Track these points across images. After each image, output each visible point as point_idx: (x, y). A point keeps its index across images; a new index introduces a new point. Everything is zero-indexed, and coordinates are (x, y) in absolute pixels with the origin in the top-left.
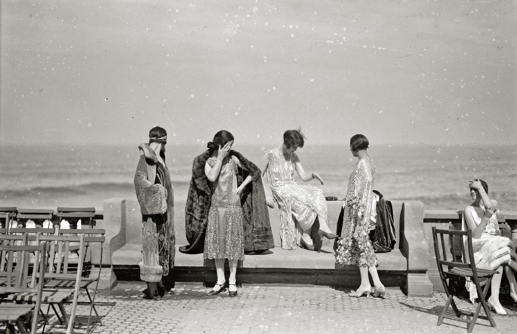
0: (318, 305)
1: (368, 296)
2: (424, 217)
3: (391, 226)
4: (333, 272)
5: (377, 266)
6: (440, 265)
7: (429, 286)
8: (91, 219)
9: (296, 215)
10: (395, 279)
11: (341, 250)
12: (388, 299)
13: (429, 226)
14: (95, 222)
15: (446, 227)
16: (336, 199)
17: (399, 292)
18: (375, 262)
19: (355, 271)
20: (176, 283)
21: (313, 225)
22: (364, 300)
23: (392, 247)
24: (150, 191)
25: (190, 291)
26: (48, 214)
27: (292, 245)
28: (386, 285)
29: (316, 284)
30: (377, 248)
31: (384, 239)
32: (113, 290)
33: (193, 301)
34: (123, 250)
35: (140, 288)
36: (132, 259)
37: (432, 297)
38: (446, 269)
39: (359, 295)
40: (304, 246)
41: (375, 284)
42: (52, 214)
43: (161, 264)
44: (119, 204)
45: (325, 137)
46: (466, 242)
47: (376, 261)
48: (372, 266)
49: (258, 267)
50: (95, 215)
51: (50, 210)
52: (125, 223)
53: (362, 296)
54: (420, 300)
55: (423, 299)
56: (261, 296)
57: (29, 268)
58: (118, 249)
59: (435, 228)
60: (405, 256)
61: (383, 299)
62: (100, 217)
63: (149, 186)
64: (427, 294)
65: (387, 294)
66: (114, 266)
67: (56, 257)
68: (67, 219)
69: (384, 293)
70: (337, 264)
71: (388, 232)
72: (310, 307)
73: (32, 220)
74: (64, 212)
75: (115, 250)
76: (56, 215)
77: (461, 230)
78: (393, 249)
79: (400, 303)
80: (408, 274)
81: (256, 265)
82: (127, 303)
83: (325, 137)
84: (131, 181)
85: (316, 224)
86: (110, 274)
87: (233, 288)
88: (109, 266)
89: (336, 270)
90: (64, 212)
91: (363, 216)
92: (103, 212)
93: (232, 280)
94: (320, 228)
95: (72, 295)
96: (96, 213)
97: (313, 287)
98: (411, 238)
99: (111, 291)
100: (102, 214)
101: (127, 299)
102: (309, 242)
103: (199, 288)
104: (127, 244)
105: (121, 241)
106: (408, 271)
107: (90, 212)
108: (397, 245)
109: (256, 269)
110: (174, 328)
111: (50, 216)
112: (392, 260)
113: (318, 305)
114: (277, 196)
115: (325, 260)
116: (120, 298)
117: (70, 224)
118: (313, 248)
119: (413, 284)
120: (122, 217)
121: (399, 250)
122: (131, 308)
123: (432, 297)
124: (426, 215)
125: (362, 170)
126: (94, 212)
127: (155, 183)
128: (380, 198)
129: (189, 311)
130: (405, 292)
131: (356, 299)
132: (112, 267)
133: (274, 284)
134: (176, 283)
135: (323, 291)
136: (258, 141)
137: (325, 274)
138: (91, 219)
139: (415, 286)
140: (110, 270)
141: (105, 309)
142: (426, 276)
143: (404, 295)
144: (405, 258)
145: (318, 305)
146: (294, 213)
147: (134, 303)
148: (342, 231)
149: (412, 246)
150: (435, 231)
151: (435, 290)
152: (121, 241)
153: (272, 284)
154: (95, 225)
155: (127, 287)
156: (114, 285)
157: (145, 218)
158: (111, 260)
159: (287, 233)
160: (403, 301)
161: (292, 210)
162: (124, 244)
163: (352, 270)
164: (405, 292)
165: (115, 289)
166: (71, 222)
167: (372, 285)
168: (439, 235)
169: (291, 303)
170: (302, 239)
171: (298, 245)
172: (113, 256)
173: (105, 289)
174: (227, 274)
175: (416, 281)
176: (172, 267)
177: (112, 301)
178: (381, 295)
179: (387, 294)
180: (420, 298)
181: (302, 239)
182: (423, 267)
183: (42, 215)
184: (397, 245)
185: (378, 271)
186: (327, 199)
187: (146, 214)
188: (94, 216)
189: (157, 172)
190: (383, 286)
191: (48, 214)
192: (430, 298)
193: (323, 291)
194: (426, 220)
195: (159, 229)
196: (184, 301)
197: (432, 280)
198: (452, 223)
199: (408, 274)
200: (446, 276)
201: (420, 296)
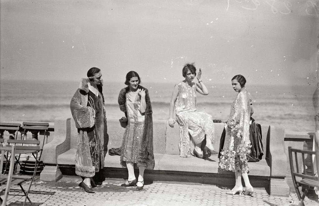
0: (202, 200)
1: (240, 194)
2: (285, 137)
3: (260, 143)
4: (215, 175)
5: (248, 172)
6: (294, 176)
7: (286, 188)
8: (46, 131)
9: (192, 132)
10: (262, 182)
11: (222, 159)
12: (256, 197)
13: (288, 144)
14: (49, 133)
15: (300, 146)
16: (220, 122)
17: (264, 191)
18: (247, 170)
19: (231, 175)
20: (106, 178)
21: (203, 141)
22: (237, 198)
23: (260, 157)
24: (83, 112)
25: (112, 184)
26: (17, 126)
27: (186, 154)
28: (254, 186)
29: (203, 183)
30: (249, 159)
31: (254, 152)
32: (58, 182)
33: (111, 193)
34: (67, 154)
35: (77, 181)
36: (71, 161)
37: (288, 197)
38: (299, 179)
39: (234, 193)
40: (196, 155)
41: (246, 185)
42: (20, 127)
43: (94, 164)
44: (65, 121)
45: (215, 76)
46: (314, 161)
47: (247, 169)
48: (244, 173)
49: (160, 170)
50: (49, 128)
51: (19, 124)
52: (70, 134)
53: (235, 194)
54: (280, 199)
55: (282, 198)
56: (162, 191)
57: (4, 163)
58: (63, 153)
59: (291, 147)
60: (268, 165)
61: (252, 196)
62: (52, 130)
63: (80, 108)
64: (285, 194)
65: (255, 193)
66: (59, 165)
67: (20, 156)
68: (30, 130)
69: (252, 193)
70: (219, 169)
71: (257, 148)
72: (196, 202)
73: (7, 130)
74: (27, 125)
75: (61, 154)
76: (22, 128)
77: (312, 150)
78: (261, 159)
79: (264, 201)
80: (271, 179)
81: (159, 168)
82: (64, 193)
83: (215, 76)
84: (69, 103)
85: (204, 142)
86: (56, 171)
87: (140, 184)
88: (55, 165)
89: (218, 174)
90: (27, 125)
91: (241, 136)
92: (54, 126)
93: (141, 178)
94: (206, 145)
95: (4, 191)
96: (49, 127)
97: (201, 185)
98: (276, 152)
99: (56, 183)
100: (53, 128)
101: (64, 190)
102: (200, 152)
103: (119, 183)
104: (71, 149)
105: (66, 147)
106: (271, 177)
107: (45, 126)
108: (264, 157)
109: (159, 171)
110: (155, 187)
111: (18, 128)
112: (259, 168)
113: (201, 200)
114: (179, 118)
115: (211, 166)
116: (60, 189)
117: (33, 134)
118: (202, 157)
119: (275, 187)
120: (67, 130)
121: (265, 160)
122: (64, 198)
123: (288, 197)
124: (287, 135)
125: (240, 100)
126: (48, 126)
127: (87, 106)
128: (252, 122)
129: (105, 201)
130: (269, 192)
131: (231, 196)
132: (57, 165)
133: (173, 182)
134: (106, 178)
135: (208, 188)
136: (162, 76)
137: (209, 176)
138: (46, 131)
139: (276, 188)
140: (56, 168)
141: (45, 198)
142: (285, 181)
143: (267, 194)
144: (269, 167)
145: (202, 200)
146: (190, 131)
147: (68, 193)
148: (224, 145)
149: (274, 159)
150: (291, 150)
151: (292, 191)
152: (66, 147)
153: (171, 182)
154: (49, 135)
155: (67, 179)
156: (60, 178)
157: (79, 130)
158: (56, 160)
159: (184, 145)
160: (267, 200)
161: (189, 128)
162: (69, 149)
163: (229, 174)
164: (269, 192)
165: (60, 181)
166: (34, 132)
167: (244, 185)
168: (293, 153)
169: (181, 197)
170: (194, 150)
171: (191, 154)
172: (58, 158)
173: (52, 181)
174: (137, 173)
175: (277, 185)
176: (102, 168)
177: (53, 191)
178: (250, 194)
179: (255, 193)
180: (279, 197)
181: (194, 150)
182: (282, 174)
183: (6, 127)
184: (264, 157)
185: (249, 176)
186: (214, 121)
187: (79, 128)
188: (47, 129)
189: (89, 99)
190: (251, 187)
191: (17, 126)
192: (287, 198)
193: (208, 188)
194: (286, 139)
195: (91, 138)
196: (105, 193)
197: (289, 183)
198: (306, 142)
199: (271, 179)
200: (298, 184)
201: (279, 196)
